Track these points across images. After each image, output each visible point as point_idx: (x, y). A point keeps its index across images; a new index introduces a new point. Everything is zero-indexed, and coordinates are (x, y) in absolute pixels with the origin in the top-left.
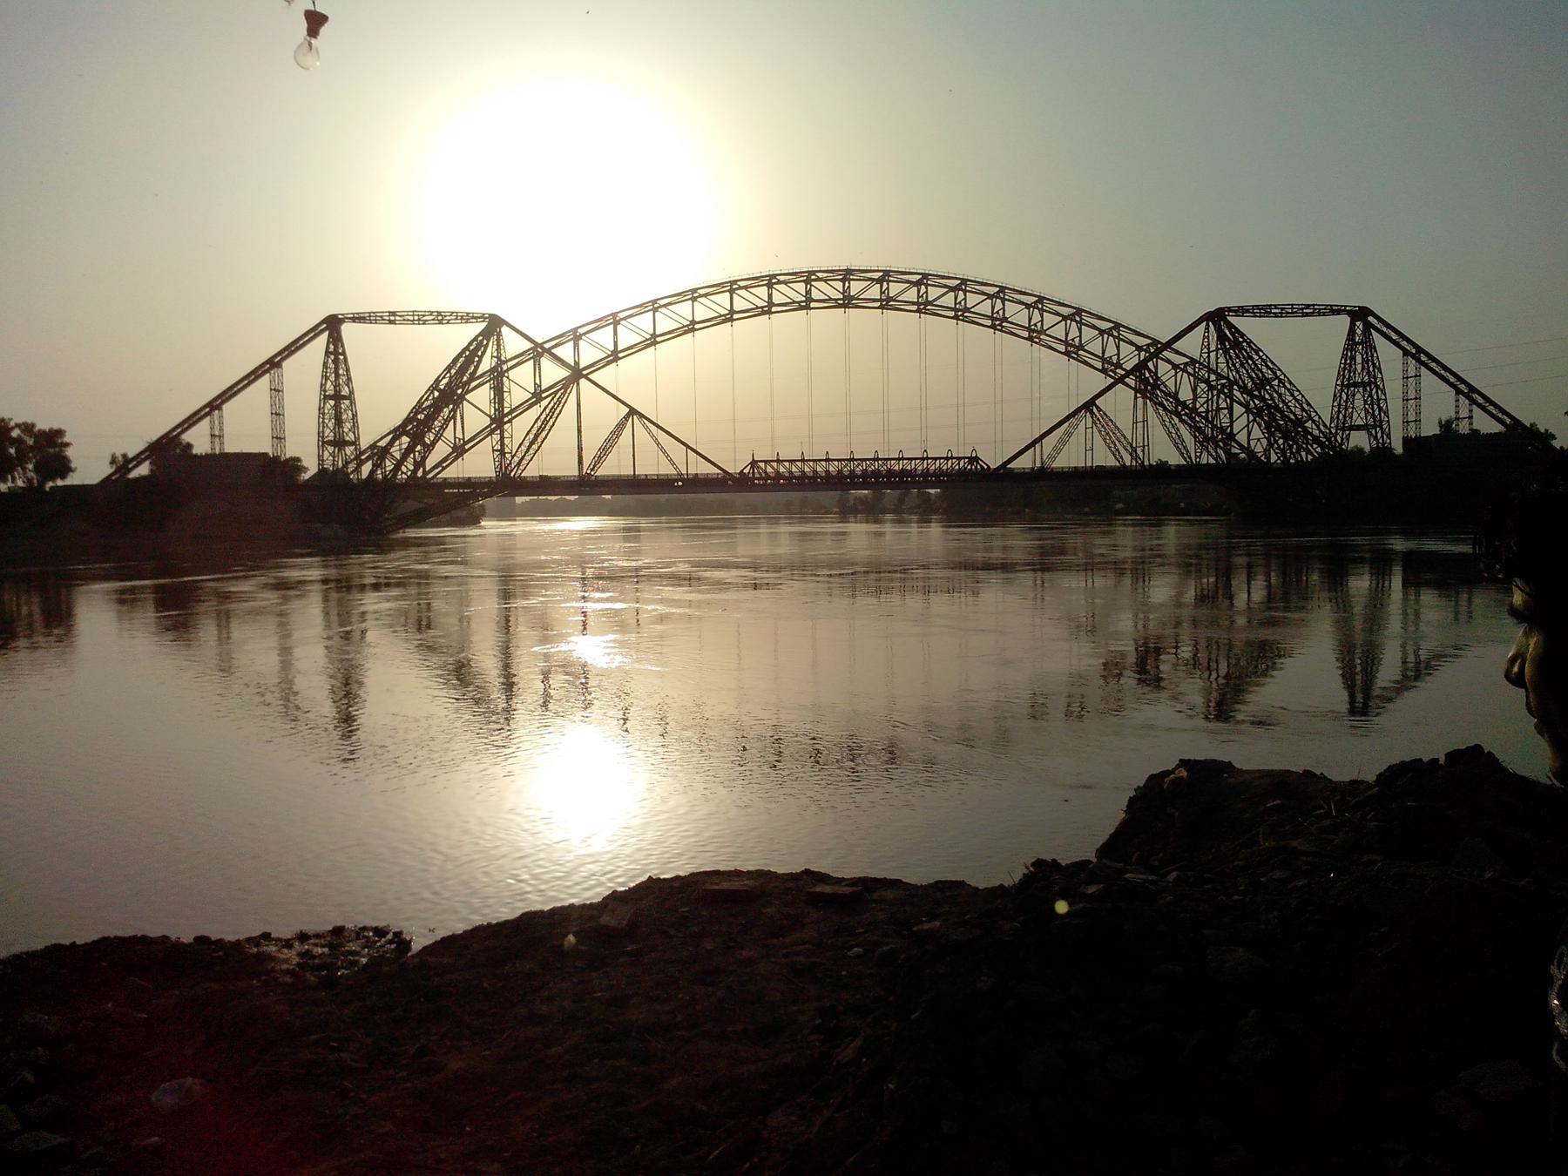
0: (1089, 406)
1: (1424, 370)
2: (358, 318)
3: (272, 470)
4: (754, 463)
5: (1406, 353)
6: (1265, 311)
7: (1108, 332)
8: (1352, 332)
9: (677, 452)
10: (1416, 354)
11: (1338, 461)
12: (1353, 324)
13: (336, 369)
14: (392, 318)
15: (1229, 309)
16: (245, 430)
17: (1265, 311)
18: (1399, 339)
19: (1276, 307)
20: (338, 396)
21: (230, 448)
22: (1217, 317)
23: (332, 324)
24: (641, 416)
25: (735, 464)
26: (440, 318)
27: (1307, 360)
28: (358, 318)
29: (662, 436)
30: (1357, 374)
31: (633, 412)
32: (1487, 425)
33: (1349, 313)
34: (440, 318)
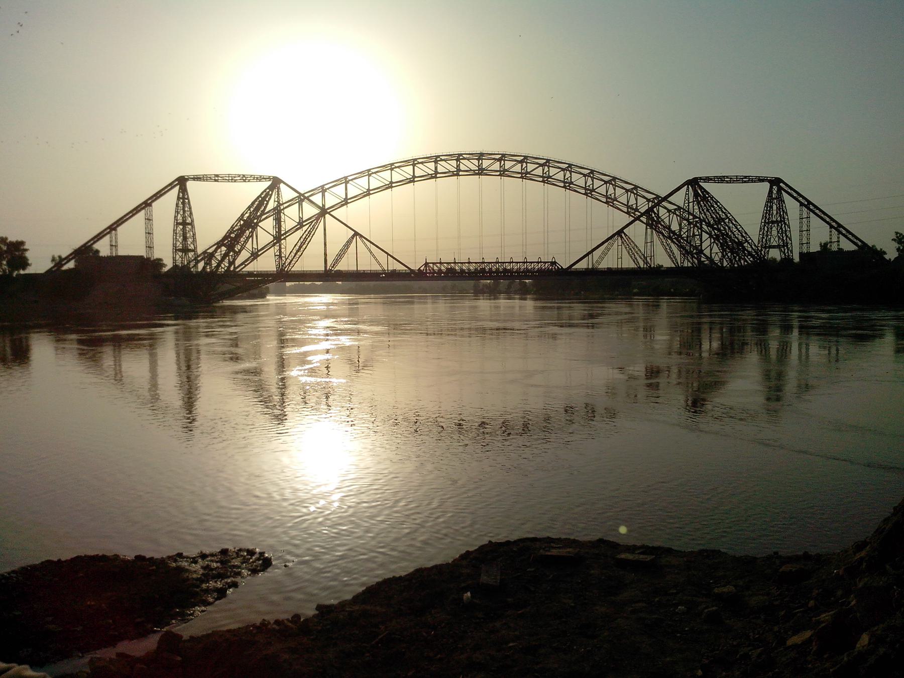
0: (620, 233)
1: (812, 214)
2: (197, 178)
3: (146, 266)
4: (426, 264)
5: (802, 204)
6: (721, 179)
7: (631, 191)
8: (771, 192)
9: (382, 257)
10: (807, 204)
11: (762, 265)
12: (771, 188)
14: (216, 178)
15: (701, 178)
16: (130, 242)
17: (721, 179)
18: (797, 195)
19: (727, 177)
20: (184, 223)
21: (122, 252)
22: (693, 183)
23: (182, 182)
26: (244, 178)
27: (745, 208)
28: (197, 178)
29: (373, 248)
30: (773, 216)
31: (356, 234)
32: (847, 246)
33: (770, 181)
34: (244, 178)
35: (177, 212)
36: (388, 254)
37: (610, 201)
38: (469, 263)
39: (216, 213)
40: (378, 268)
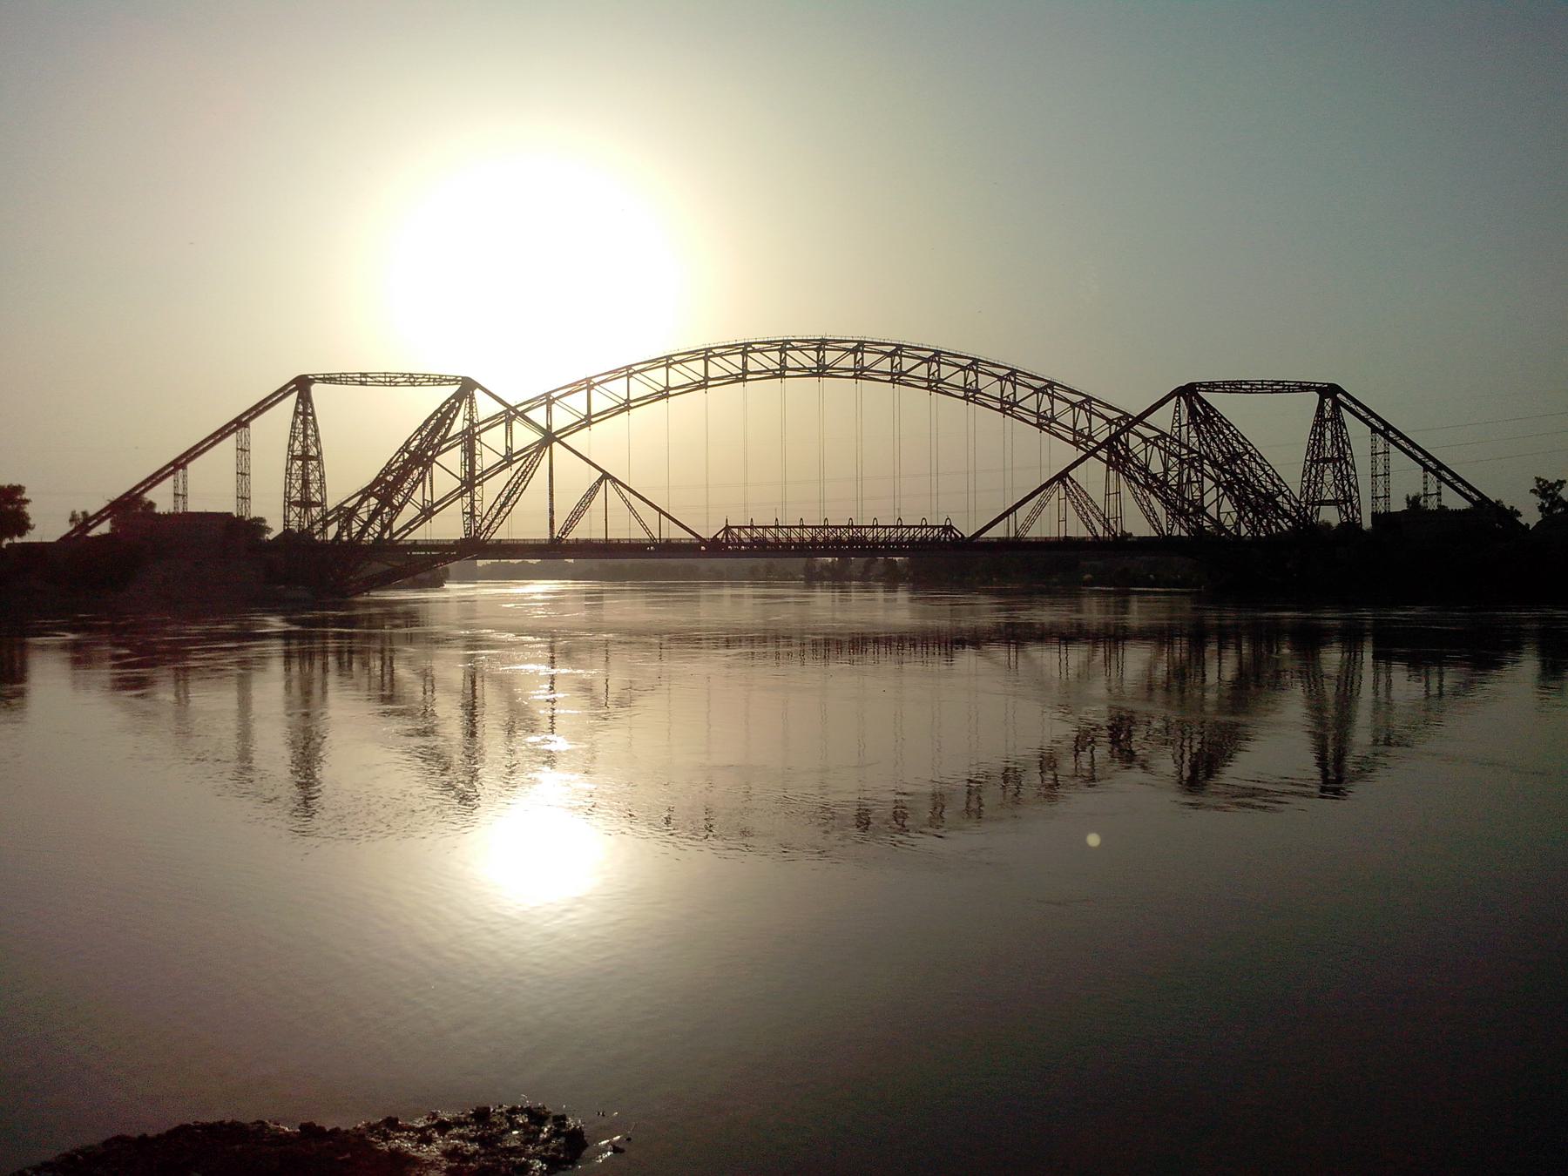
0: (1062, 477)
2: (329, 379)
3: (236, 531)
4: (727, 529)
5: (1374, 430)
6: (1235, 387)
8: (1321, 408)
9: (650, 516)
10: (1384, 430)
11: (1308, 532)
12: (1322, 401)
13: (305, 429)
14: (363, 379)
15: (1201, 385)
16: (209, 489)
17: (1235, 387)
18: (1367, 416)
20: (305, 457)
22: (1188, 392)
23: (302, 385)
24: (615, 480)
25: (709, 530)
26: (412, 380)
27: (1278, 435)
28: (329, 379)
29: (633, 500)
30: (1328, 450)
31: (606, 476)
32: (1455, 501)
33: (1319, 390)
34: (412, 380)
35: (293, 437)
36: (661, 512)
37: (1045, 422)
38: (802, 527)
39: (362, 438)
40: (640, 535)
